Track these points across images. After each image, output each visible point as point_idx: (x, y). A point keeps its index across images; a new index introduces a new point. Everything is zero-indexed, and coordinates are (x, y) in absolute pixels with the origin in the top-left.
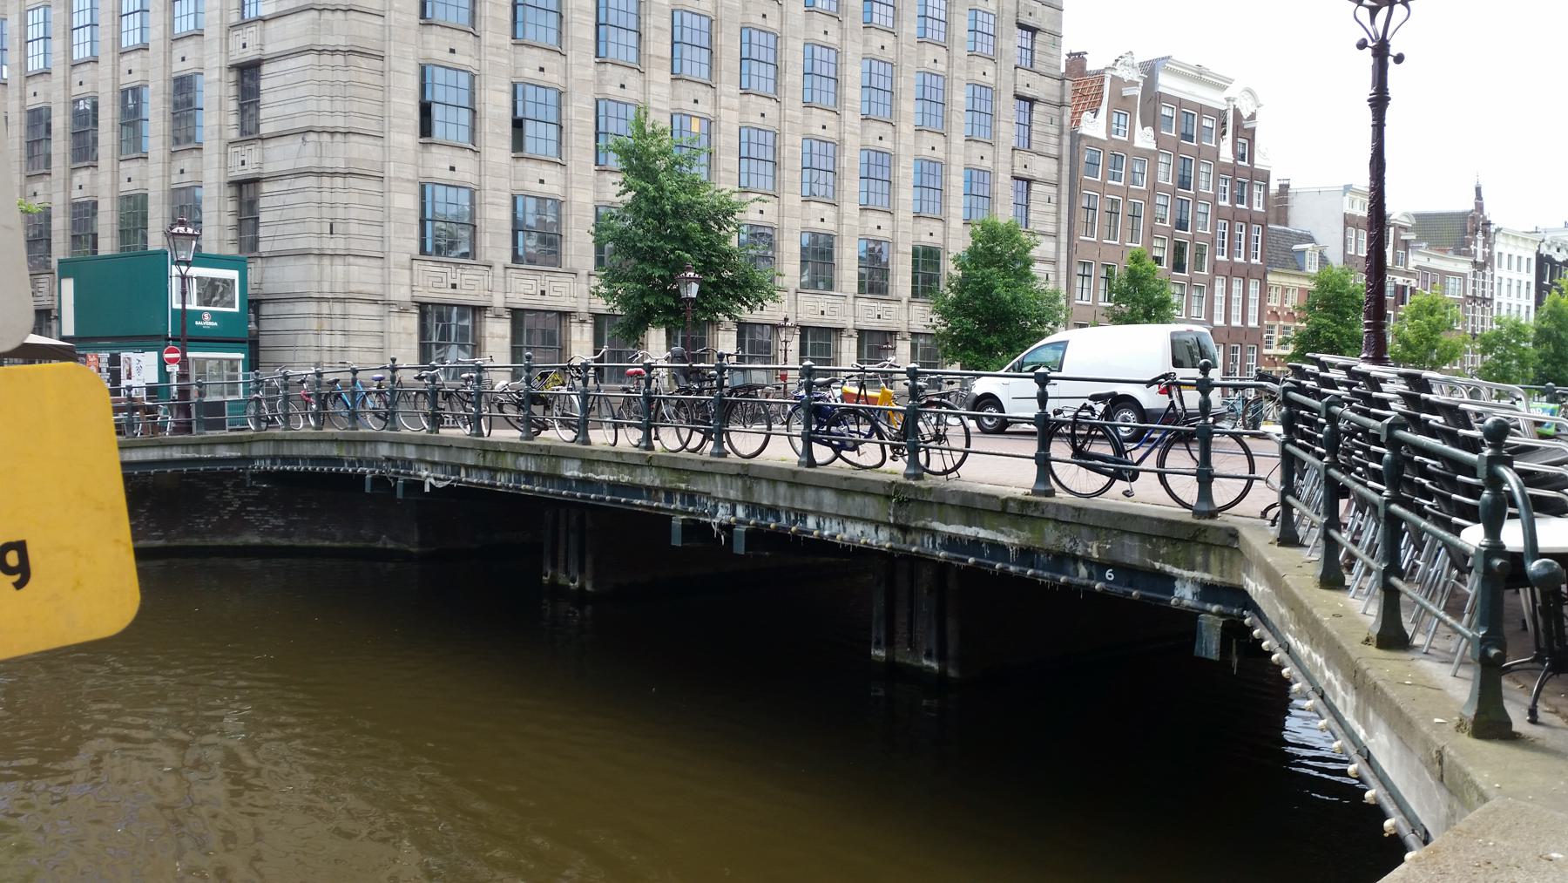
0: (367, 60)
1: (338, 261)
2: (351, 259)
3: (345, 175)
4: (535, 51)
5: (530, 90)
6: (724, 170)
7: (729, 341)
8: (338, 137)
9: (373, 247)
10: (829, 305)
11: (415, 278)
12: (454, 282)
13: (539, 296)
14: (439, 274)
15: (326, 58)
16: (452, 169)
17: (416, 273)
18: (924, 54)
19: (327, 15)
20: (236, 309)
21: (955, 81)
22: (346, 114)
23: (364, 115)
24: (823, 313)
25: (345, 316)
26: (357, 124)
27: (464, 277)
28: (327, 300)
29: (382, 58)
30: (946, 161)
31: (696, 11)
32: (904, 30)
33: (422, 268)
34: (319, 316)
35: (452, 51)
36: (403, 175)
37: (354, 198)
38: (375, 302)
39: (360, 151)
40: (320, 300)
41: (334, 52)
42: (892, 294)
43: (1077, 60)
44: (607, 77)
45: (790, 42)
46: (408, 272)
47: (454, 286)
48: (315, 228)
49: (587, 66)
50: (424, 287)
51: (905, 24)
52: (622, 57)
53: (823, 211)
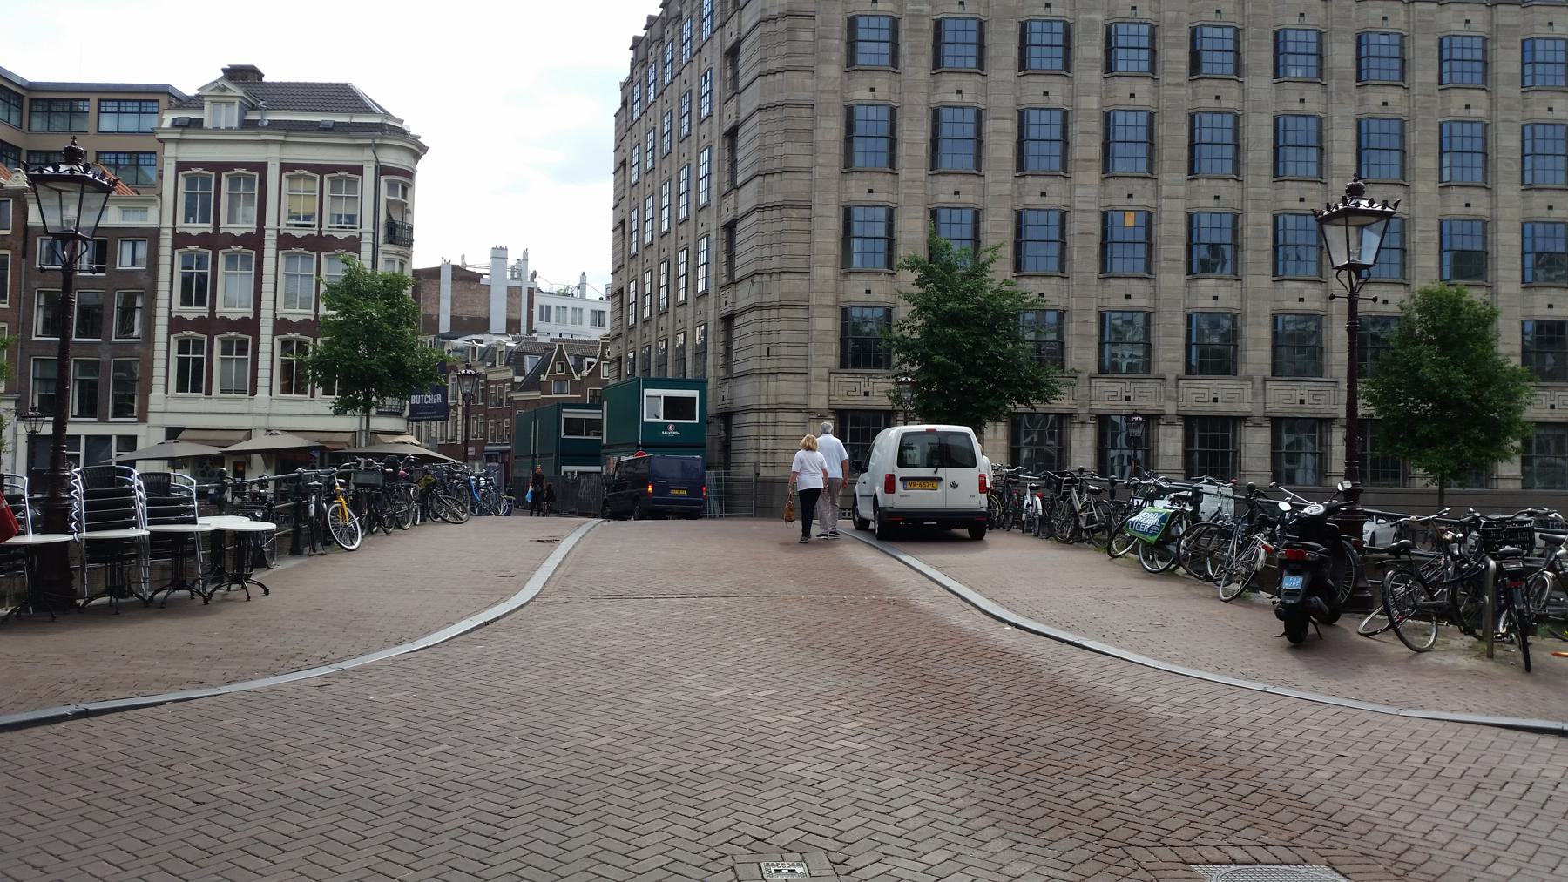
0: (797, 211)
1: (772, 378)
2: (780, 376)
3: (780, 306)
4: (951, 178)
5: (1291, 221)
6: (1165, 259)
7: (1172, 436)
8: (774, 276)
9: (799, 364)
10: (1311, 393)
11: (832, 389)
12: (1128, 394)
13: (1298, 406)
14: (853, 384)
15: (767, 214)
16: (868, 292)
17: (832, 384)
18: (1450, 101)
19: (768, 178)
20: (697, 421)
21: (1500, 124)
22: (780, 257)
23: (794, 256)
24: (1302, 402)
25: (775, 424)
26: (788, 263)
27: (875, 385)
28: (764, 411)
29: (810, 207)
30: (1491, 217)
31: (1131, 108)
32: (1417, 80)
33: (1098, 384)
34: (758, 424)
35: (870, 191)
36: (825, 302)
37: (785, 325)
38: (799, 411)
39: (790, 286)
40: (760, 411)
41: (772, 208)
42: (1243, 371)
43: (646, 28)
44: (1027, 188)
45: (1253, 119)
46: (826, 384)
47: (867, 394)
48: (756, 351)
49: (1005, 182)
50: (839, 396)
51: (1418, 73)
52: (1467, 178)
53: (1301, 290)
